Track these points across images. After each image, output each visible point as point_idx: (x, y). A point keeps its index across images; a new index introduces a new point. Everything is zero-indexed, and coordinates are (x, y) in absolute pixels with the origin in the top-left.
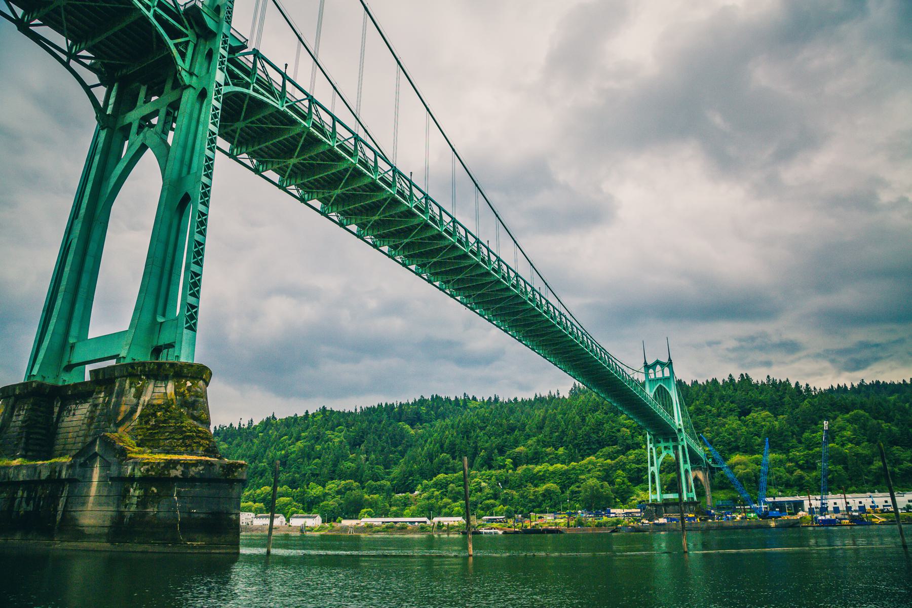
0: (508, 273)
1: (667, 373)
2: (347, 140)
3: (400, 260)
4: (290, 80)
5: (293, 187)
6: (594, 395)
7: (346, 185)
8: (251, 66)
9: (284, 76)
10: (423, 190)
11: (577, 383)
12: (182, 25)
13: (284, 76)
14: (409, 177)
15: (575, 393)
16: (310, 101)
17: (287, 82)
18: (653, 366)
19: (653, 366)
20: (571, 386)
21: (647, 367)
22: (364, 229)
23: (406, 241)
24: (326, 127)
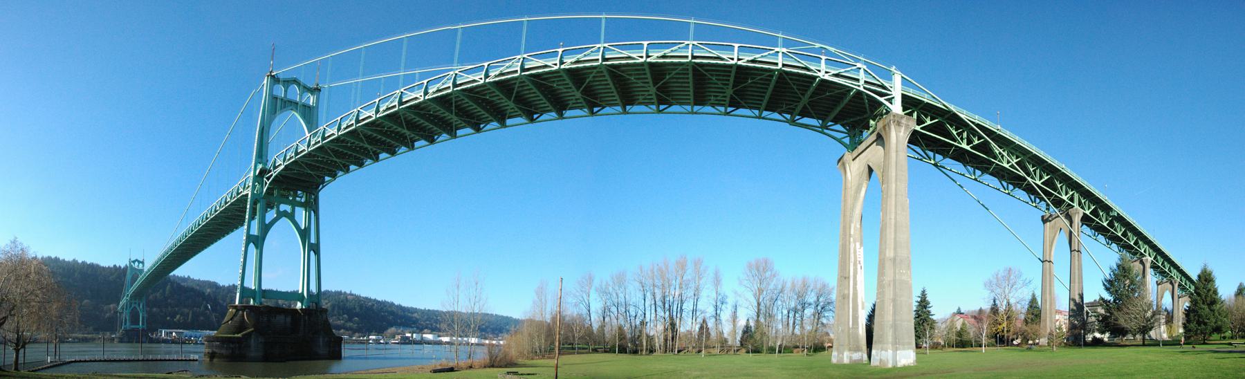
1: (311, 100)
18: (287, 83)
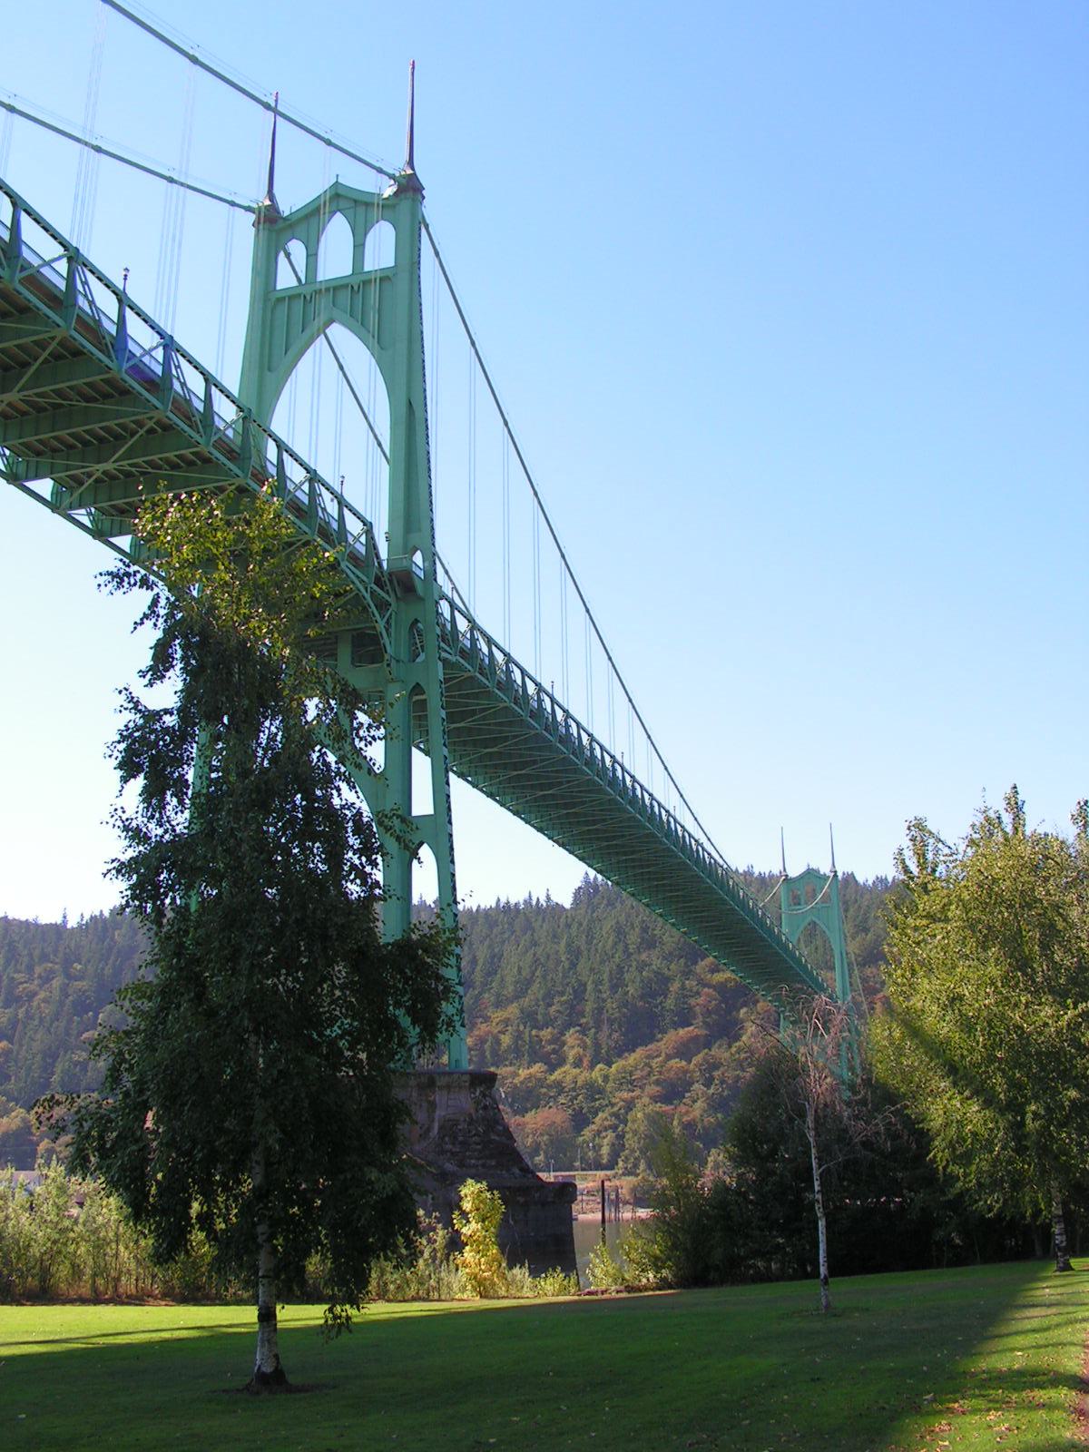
0: (208, 400)
1: (382, 248)
2: (48, 264)
3: (86, 521)
4: (352, 510)
6: (632, 910)
7: (37, 380)
8: (62, 285)
9: (122, 299)
10: (362, 512)
11: (592, 873)
12: (382, 589)
13: (122, 299)
14: (337, 488)
15: (586, 894)
16: (70, 260)
17: (285, 455)
18: (309, 222)
19: (309, 222)
20: (578, 882)
21: (274, 226)
22: (71, 490)
23: (99, 469)
24: (194, 399)
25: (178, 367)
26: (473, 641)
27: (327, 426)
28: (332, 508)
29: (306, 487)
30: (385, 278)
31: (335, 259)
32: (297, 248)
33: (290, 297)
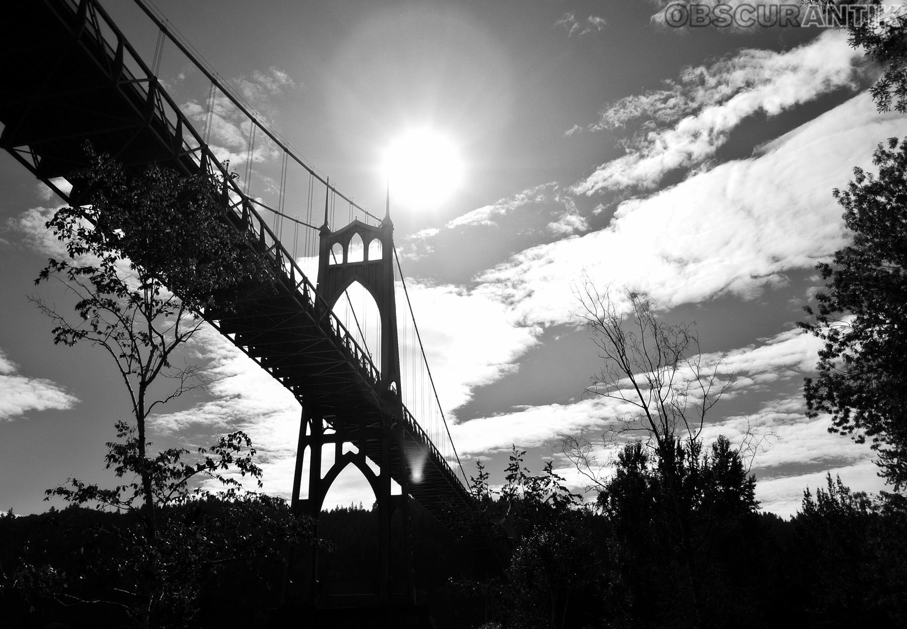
0: (292, 273)
1: (376, 252)
5: (26, 148)
19: (344, 237)
25: (159, 100)
26: (305, 290)
27: (355, 313)
28: (257, 228)
29: (302, 285)
30: (376, 263)
31: (356, 255)
32: (337, 247)
33: (337, 267)
